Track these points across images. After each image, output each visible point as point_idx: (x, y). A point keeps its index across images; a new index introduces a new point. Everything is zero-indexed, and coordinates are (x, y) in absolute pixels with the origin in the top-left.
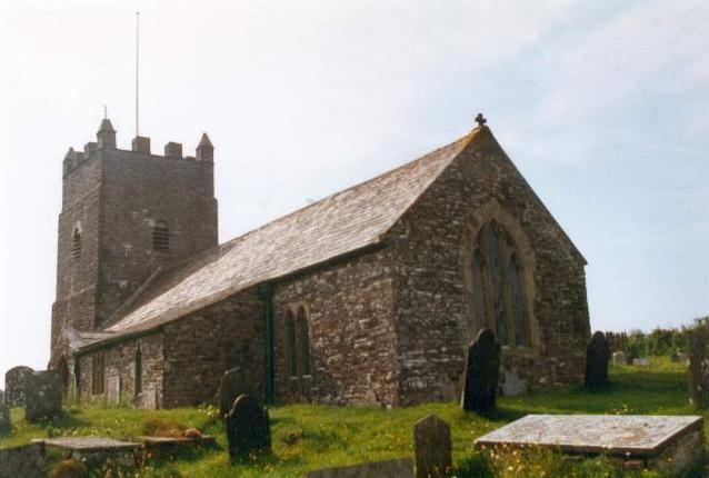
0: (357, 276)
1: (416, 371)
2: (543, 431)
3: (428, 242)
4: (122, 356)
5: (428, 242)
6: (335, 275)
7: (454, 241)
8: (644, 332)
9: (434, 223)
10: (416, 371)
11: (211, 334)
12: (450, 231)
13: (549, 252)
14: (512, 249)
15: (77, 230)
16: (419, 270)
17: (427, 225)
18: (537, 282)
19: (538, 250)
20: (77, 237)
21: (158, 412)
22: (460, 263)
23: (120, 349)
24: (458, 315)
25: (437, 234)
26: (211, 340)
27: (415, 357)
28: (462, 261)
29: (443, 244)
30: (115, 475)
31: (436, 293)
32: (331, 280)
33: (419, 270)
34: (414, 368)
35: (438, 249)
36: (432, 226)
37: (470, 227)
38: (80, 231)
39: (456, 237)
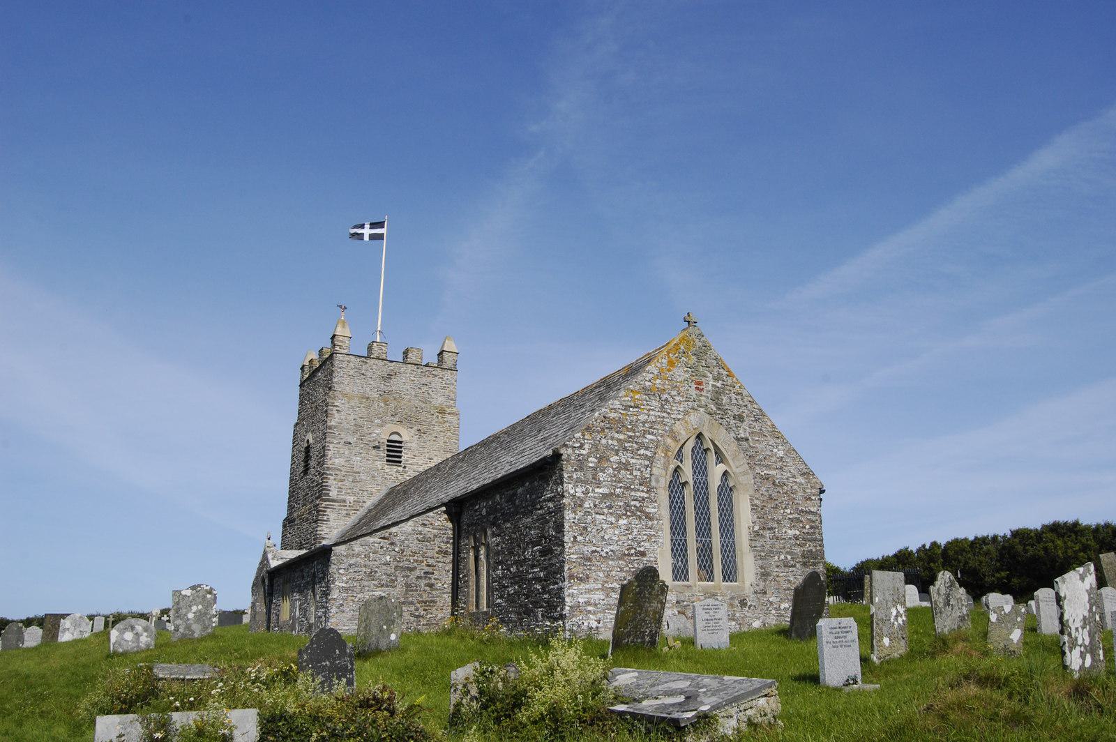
0: (534, 497)
1: (590, 608)
2: (840, 643)
3: (614, 458)
4: (303, 577)
5: (614, 458)
6: (515, 494)
7: (646, 457)
8: (938, 542)
9: (622, 437)
10: (590, 608)
11: (388, 557)
12: (641, 446)
13: (773, 472)
14: (721, 468)
15: (308, 441)
16: (600, 491)
17: (612, 438)
18: (754, 508)
19: (758, 469)
20: (308, 449)
21: (674, 582)
22: (653, 484)
23: (302, 571)
24: (647, 544)
25: (625, 449)
26: (387, 564)
27: (589, 591)
28: (657, 481)
29: (633, 461)
30: (211, 741)
31: (620, 517)
32: (511, 500)
33: (600, 491)
34: (588, 603)
35: (626, 466)
36: (619, 440)
37: (669, 441)
38: (311, 441)
39: (649, 453)
